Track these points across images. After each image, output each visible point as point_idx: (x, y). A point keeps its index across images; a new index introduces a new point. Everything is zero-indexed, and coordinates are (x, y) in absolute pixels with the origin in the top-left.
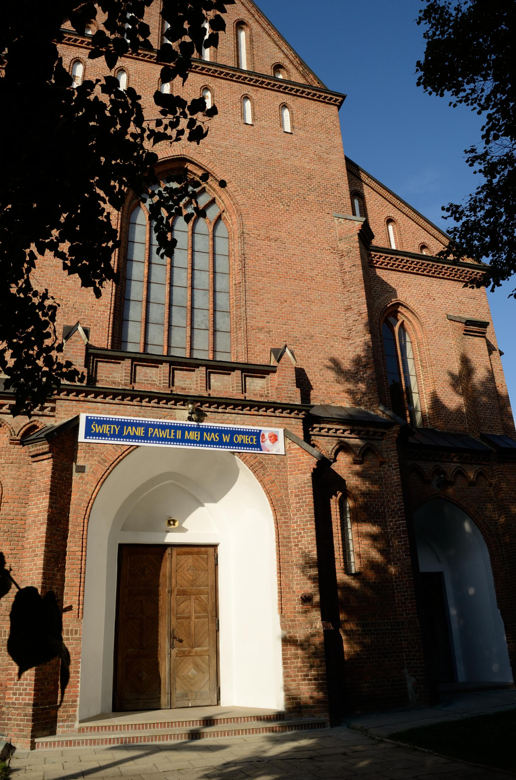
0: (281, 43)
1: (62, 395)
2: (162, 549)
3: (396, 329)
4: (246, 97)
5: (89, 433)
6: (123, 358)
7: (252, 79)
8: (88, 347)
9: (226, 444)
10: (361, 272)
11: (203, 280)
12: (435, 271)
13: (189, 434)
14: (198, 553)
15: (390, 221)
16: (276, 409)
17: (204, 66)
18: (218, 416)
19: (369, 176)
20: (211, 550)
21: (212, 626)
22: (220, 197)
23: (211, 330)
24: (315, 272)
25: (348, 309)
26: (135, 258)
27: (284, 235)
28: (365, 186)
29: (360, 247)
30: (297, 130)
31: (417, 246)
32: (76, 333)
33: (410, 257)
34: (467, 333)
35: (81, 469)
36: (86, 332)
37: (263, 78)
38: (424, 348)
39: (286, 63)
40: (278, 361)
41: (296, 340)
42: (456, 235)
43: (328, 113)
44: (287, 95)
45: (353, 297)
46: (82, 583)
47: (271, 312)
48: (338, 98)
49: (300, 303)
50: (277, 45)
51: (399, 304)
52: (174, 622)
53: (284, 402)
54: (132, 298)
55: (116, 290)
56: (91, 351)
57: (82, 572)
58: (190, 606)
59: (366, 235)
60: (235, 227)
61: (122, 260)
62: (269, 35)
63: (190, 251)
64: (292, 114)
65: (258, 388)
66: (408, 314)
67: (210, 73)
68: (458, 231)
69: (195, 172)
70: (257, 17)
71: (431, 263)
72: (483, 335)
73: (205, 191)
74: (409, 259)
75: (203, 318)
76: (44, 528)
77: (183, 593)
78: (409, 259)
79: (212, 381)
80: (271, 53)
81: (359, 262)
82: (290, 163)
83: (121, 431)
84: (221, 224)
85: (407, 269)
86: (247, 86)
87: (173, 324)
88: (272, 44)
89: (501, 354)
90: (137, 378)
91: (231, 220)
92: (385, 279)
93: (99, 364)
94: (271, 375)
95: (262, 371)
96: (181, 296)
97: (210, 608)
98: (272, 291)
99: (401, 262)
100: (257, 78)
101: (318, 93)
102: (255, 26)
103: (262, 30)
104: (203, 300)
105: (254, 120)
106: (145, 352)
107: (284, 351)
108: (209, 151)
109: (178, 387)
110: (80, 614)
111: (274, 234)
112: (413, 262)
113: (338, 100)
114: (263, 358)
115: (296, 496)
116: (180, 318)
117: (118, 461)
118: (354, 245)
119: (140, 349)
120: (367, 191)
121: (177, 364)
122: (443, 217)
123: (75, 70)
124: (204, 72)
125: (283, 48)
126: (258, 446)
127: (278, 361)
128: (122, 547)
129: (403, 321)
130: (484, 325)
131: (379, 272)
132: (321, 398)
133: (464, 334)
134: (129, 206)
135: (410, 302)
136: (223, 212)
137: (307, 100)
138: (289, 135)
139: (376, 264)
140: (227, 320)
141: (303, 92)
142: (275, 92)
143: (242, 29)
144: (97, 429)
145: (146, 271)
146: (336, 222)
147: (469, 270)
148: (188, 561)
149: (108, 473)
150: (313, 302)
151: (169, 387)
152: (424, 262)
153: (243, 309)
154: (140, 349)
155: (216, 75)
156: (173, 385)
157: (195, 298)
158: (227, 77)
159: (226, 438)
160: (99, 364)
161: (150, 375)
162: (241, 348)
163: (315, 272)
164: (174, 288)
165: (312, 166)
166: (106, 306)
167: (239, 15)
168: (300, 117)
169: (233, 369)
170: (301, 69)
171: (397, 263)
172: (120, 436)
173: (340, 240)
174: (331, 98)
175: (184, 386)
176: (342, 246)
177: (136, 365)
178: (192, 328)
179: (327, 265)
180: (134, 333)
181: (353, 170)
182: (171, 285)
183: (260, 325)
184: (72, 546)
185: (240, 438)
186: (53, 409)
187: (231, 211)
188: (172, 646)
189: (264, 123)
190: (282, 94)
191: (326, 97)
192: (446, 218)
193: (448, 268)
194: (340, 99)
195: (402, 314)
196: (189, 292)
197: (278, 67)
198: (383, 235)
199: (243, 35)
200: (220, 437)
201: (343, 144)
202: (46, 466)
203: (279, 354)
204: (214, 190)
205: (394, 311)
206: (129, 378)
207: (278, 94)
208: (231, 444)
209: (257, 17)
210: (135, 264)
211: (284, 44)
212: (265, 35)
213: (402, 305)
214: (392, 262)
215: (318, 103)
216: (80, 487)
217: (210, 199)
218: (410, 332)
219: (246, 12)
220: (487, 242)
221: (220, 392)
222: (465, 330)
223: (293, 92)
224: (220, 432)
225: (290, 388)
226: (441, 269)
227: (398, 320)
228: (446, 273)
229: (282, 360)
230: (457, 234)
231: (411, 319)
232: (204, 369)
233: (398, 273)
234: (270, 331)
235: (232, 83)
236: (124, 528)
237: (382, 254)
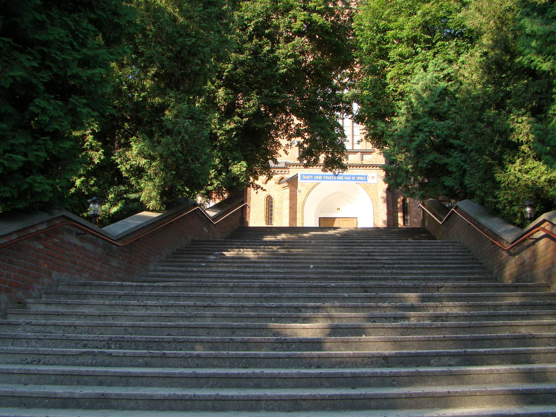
1: (291, 167)
5: (302, 179)
9: (353, 180)
13: (456, 190)
16: (373, 167)
35: (300, 191)
76: (288, 210)
83: (313, 178)
115: (394, 14)
117: (313, 188)
126: (366, 180)
128: (320, 218)
144: (304, 177)
149: (309, 192)
159: (353, 178)
169: (357, 152)
172: (313, 179)
185: (359, 178)
186: (289, 172)
200: (351, 178)
202: (287, 191)
208: (356, 180)
216: (300, 197)
220: (215, 162)
224: (351, 176)
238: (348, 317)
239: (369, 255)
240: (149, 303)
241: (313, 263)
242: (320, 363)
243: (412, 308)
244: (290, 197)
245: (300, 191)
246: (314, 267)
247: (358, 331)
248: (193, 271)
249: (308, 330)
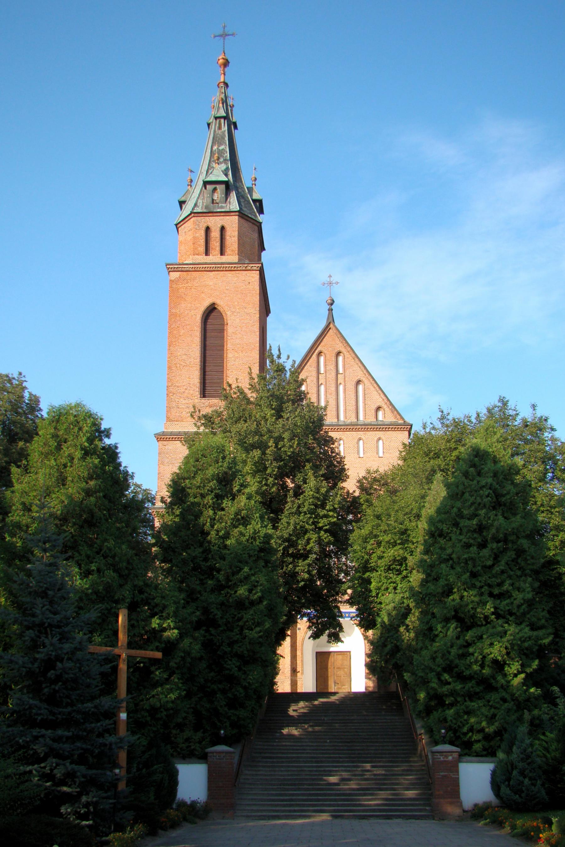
2: (329, 653)
14: (344, 654)
18: (344, 607)
20: (348, 653)
21: (349, 679)
35: (299, 629)
39: (343, 350)
46: (303, 664)
52: (335, 678)
57: (302, 661)
58: (341, 673)
76: (290, 648)
77: (339, 668)
97: (348, 673)
110: (302, 673)
128: (317, 653)
148: (340, 657)
184: (299, 653)
188: (335, 686)
194: (409, 427)
236: (317, 646)
238: (345, 775)
239: (357, 732)
240: (282, 769)
241: (329, 739)
242: (338, 790)
243: (368, 771)
244: (296, 651)
245: (299, 629)
246: (330, 742)
247: (349, 780)
248: (273, 746)
249: (333, 779)
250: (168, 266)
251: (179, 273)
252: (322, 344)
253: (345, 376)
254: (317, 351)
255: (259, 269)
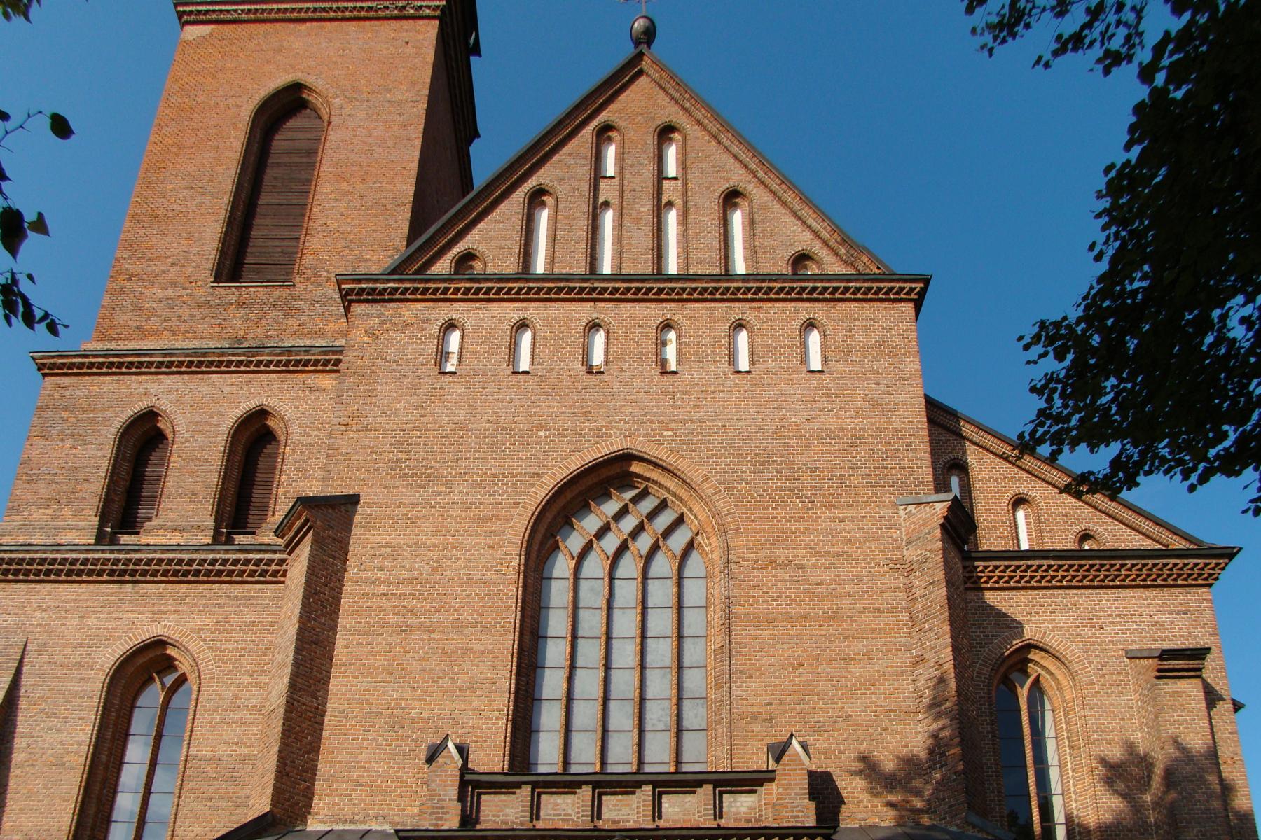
0: (805, 212)
3: (1023, 693)
4: (739, 325)
6: (518, 785)
7: (749, 289)
8: (464, 770)
10: (943, 591)
11: (660, 652)
12: (1106, 576)
15: (1019, 501)
17: (662, 286)
19: (980, 427)
22: (691, 511)
23: (674, 730)
24: (859, 607)
25: (919, 661)
26: (550, 634)
27: (801, 553)
28: (970, 449)
29: (944, 549)
30: (831, 364)
31: (1071, 538)
32: (445, 753)
33: (1055, 558)
34: (1162, 674)
36: (462, 750)
37: (770, 281)
38: (1075, 717)
39: (680, 119)
40: (778, 760)
41: (818, 727)
42: (1055, 390)
43: (895, 319)
44: (816, 304)
45: (929, 639)
47: (775, 686)
48: (913, 285)
49: (827, 664)
50: (800, 218)
51: (1030, 647)
53: (785, 825)
54: (544, 697)
55: (517, 684)
56: (468, 777)
59: (959, 526)
60: (716, 556)
61: (527, 637)
62: (784, 203)
63: (639, 610)
64: (824, 336)
65: (743, 809)
66: (1048, 663)
67: (673, 296)
68: (1058, 381)
69: (647, 475)
70: (761, 174)
71: (1098, 562)
72: (1196, 673)
73: (666, 506)
74: (1052, 562)
75: (661, 713)
78: (1052, 562)
79: (665, 805)
80: (793, 234)
81: (940, 575)
82: (817, 425)
84: (695, 556)
85: (1049, 581)
86: (740, 305)
87: (611, 727)
88: (789, 219)
89: (1237, 707)
90: (542, 813)
91: (711, 544)
92: (1003, 607)
93: (483, 797)
94: (766, 786)
95: (750, 782)
96: (624, 683)
98: (777, 651)
99: (1036, 571)
100: (759, 285)
101: (875, 285)
102: (757, 193)
103: (771, 198)
104: (660, 685)
105: (752, 362)
106: (565, 771)
107: (788, 744)
108: (670, 433)
109: (608, 820)
111: (782, 555)
112: (1060, 567)
113: (916, 292)
114: (754, 759)
116: (622, 717)
118: (930, 548)
119: (558, 769)
120: (973, 457)
121: (606, 784)
122: (1028, 363)
123: (448, 342)
124: (662, 296)
125: (810, 221)
127: (778, 760)
129: (1039, 676)
130: (1200, 654)
131: (991, 597)
132: (861, 816)
133: (1157, 678)
134: (539, 551)
135: (1053, 641)
136: (697, 534)
137: (852, 305)
138: (818, 376)
139: (986, 582)
140: (702, 711)
141: (847, 289)
142: (793, 304)
143: (735, 205)
145: (568, 650)
146: (902, 513)
147: (1177, 561)
150: (852, 659)
151: (592, 821)
152: (1083, 562)
153: (726, 689)
154: (558, 769)
155: (685, 296)
156: (599, 818)
157: (648, 683)
158: (706, 296)
160: (483, 797)
161: (564, 806)
162: (722, 752)
163: (859, 607)
164: (613, 672)
165: (859, 423)
166: (500, 710)
167: (728, 180)
168: (839, 338)
169: (699, 784)
170: (843, 251)
171: (1029, 574)
173: (909, 543)
174: (902, 289)
175: (617, 818)
176: (912, 554)
177: (539, 794)
178: (642, 731)
179: (882, 592)
180: (548, 753)
181: (942, 421)
182: (607, 668)
183: (755, 709)
187: (709, 530)
189: (771, 364)
190: (807, 305)
191: (891, 289)
192: (1035, 362)
193: (1133, 566)
194: (919, 286)
195: (1036, 663)
196: (638, 674)
197: (801, 259)
198: (1005, 530)
199: (737, 219)
201: (923, 370)
203: (779, 751)
204: (681, 500)
205: (1020, 660)
206: (528, 814)
207: (799, 305)
209: (761, 174)
210: (550, 643)
211: (811, 212)
212: (776, 206)
213: (1037, 647)
214: (1019, 573)
215: (876, 305)
217: (656, 502)
218: (1051, 693)
219: (742, 171)
221: (674, 821)
222: (1159, 671)
223: (827, 296)
225: (798, 802)
226: (1119, 570)
227: (1028, 676)
228: (1127, 576)
229: (785, 759)
230: (1056, 389)
231: (1052, 669)
232: (650, 788)
233: (1030, 592)
234: (771, 718)
235: (713, 305)
237: (998, 563)
250: (181, 9)
251: (213, 26)
252: (613, 107)
253: (685, 185)
254: (594, 123)
255: (438, 13)
